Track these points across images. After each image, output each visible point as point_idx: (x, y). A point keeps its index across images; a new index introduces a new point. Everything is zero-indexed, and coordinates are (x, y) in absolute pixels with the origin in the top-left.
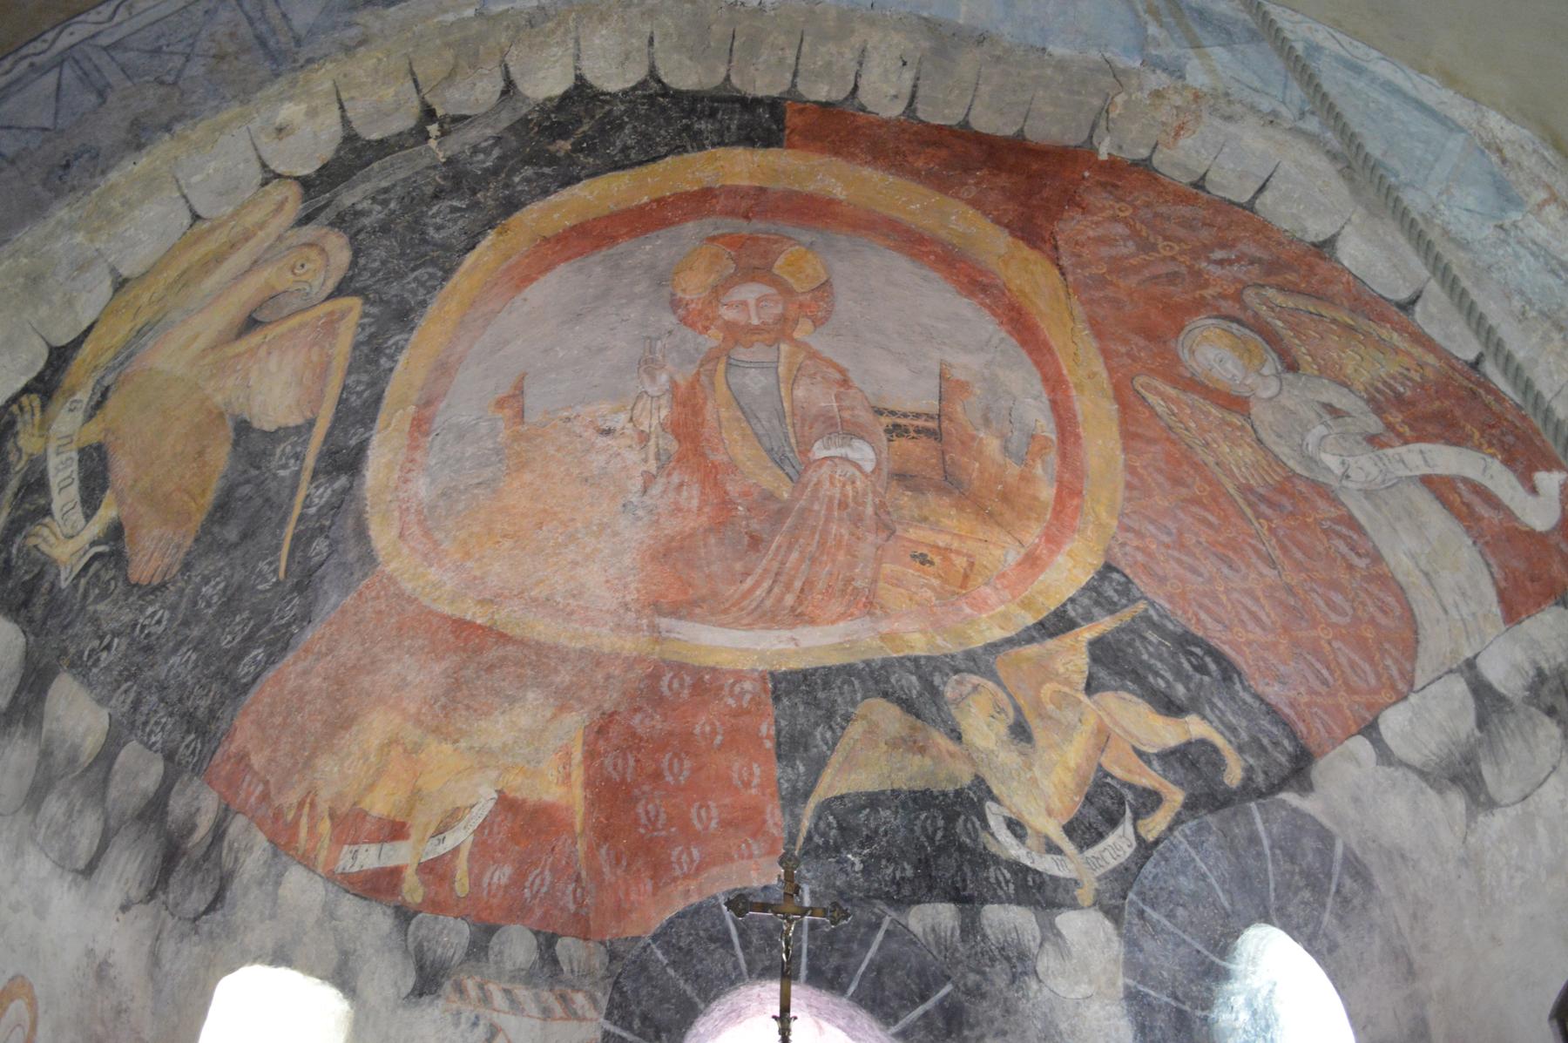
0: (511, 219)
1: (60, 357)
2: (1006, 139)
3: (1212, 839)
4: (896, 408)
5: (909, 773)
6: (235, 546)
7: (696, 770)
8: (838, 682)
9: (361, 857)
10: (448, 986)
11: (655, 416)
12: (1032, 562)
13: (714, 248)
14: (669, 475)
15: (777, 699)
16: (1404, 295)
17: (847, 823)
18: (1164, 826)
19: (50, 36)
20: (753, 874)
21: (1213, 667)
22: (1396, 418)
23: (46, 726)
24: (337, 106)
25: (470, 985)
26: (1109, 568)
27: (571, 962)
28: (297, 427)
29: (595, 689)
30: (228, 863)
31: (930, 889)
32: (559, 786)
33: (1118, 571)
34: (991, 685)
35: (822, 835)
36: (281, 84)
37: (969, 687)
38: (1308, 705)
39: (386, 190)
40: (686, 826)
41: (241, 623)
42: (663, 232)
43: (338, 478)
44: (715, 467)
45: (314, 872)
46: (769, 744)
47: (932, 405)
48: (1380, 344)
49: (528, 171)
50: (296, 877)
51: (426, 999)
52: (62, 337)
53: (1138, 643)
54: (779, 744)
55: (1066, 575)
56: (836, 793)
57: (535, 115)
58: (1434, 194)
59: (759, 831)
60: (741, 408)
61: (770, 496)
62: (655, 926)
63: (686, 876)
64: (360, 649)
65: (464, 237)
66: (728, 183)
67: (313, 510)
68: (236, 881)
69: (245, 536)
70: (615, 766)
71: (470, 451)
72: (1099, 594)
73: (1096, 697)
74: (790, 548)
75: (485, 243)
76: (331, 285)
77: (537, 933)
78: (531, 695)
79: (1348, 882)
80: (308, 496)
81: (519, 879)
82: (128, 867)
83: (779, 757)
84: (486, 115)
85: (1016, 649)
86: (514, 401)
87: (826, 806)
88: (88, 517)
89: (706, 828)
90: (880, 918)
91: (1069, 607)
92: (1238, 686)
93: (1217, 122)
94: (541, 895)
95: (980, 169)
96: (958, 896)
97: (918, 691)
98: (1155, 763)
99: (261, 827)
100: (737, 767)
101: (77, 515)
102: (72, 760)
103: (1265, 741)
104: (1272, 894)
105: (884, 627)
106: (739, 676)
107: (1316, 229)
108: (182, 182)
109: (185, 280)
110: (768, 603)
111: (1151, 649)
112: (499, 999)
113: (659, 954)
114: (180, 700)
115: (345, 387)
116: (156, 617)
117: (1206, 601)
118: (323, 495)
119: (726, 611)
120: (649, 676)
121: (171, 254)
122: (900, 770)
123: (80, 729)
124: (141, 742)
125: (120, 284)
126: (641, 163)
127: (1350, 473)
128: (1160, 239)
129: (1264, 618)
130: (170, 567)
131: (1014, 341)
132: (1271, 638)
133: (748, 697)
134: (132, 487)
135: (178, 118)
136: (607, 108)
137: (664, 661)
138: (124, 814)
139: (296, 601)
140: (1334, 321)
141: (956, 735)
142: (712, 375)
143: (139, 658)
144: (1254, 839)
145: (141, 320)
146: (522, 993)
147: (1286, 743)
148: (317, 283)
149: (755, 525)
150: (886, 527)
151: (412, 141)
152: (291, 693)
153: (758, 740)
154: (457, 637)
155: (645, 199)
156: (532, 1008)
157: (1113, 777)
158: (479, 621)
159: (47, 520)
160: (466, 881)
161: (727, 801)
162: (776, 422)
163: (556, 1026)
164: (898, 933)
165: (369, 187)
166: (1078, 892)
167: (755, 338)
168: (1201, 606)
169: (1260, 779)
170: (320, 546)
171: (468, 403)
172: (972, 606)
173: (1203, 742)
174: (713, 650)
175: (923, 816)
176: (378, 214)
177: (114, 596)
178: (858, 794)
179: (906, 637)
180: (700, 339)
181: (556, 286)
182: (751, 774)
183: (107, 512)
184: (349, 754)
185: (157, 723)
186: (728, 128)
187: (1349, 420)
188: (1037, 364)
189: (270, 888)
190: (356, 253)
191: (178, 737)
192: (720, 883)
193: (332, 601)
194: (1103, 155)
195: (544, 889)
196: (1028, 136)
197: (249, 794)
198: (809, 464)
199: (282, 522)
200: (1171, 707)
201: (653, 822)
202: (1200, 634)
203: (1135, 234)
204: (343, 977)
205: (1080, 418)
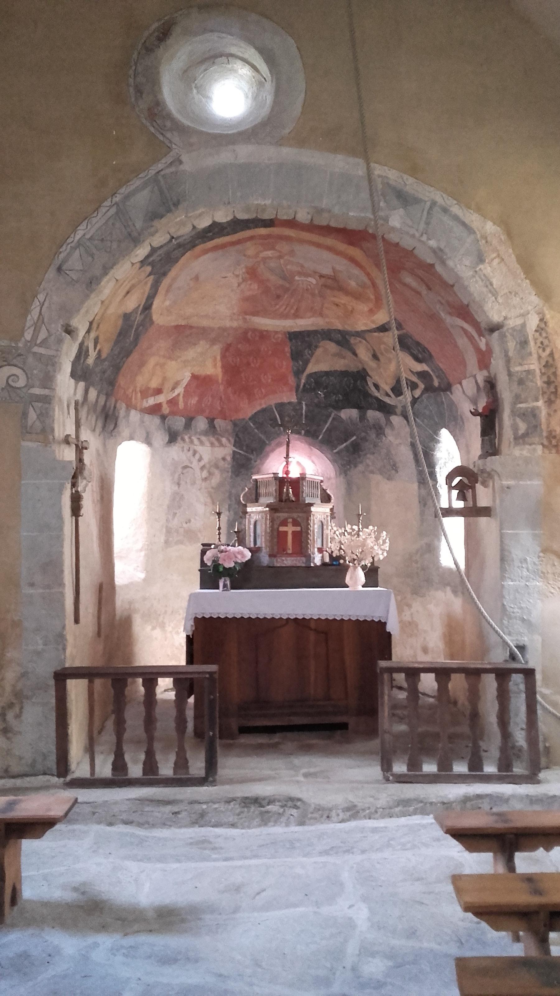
1: (91, 323)
5: (340, 365)
10: (179, 438)
17: (318, 381)
19: (72, 236)
20: (285, 398)
25: (186, 437)
27: (220, 427)
30: (117, 414)
32: (212, 368)
34: (364, 341)
35: (309, 385)
36: (137, 248)
37: (357, 341)
46: (288, 355)
50: (133, 412)
51: (172, 443)
52: (91, 319)
54: (292, 354)
56: (314, 371)
62: (250, 415)
70: (233, 361)
77: (207, 418)
78: (201, 342)
81: (200, 402)
87: (310, 376)
97: (343, 339)
105: (327, 320)
106: (276, 332)
113: (252, 425)
118: (142, 317)
133: (280, 339)
141: (355, 354)
144: (442, 403)
146: (203, 438)
150: (322, 296)
160: (183, 404)
163: (216, 449)
164: (337, 419)
173: (427, 371)
175: (346, 379)
192: (272, 401)
200: (418, 360)
204: (148, 441)
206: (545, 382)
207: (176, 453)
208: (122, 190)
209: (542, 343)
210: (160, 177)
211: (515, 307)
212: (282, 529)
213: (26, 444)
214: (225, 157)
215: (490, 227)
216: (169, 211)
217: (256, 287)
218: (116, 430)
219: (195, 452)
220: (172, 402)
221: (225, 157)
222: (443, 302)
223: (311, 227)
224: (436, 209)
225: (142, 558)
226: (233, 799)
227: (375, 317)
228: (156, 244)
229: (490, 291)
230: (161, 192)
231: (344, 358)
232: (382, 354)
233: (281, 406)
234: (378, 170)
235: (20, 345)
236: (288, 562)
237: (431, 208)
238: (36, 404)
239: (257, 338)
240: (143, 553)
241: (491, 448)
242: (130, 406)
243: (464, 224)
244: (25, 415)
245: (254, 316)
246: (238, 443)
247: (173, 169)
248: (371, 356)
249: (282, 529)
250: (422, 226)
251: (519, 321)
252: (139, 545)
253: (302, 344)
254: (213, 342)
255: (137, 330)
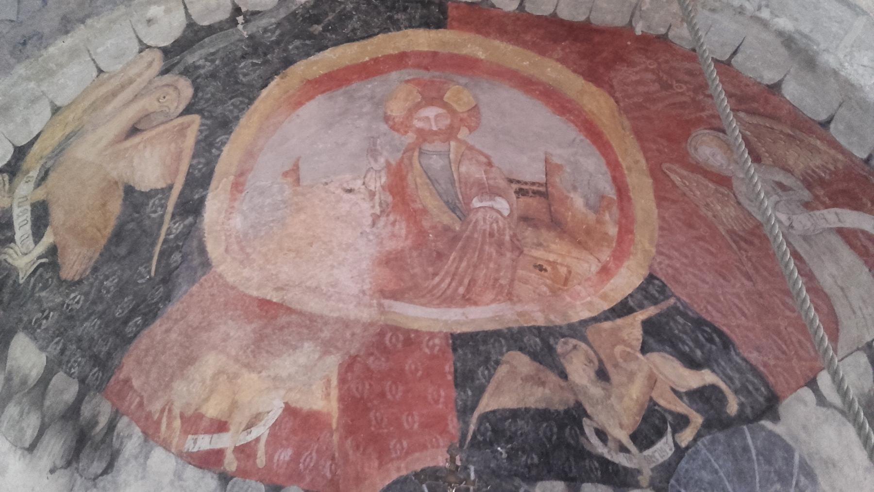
0: (288, 70)
1: (20, 152)
2: (579, 23)
3: (720, 448)
4: (520, 179)
5: (535, 397)
6: (124, 258)
8: (492, 341)
9: (198, 443)
11: (378, 181)
12: (605, 272)
13: (410, 86)
14: (388, 215)
15: (455, 350)
16: (823, 117)
17: (498, 426)
18: (691, 439)
21: (717, 340)
22: (821, 192)
23: (8, 364)
24: (182, 7)
26: (651, 278)
28: (162, 189)
29: (345, 342)
30: (116, 444)
31: (549, 472)
32: (323, 400)
33: (658, 279)
34: (583, 345)
35: (483, 435)
37: (570, 346)
38: (775, 366)
39: (213, 54)
41: (128, 301)
42: (377, 78)
43: (187, 218)
44: (415, 211)
45: (170, 451)
46: (450, 378)
47: (541, 178)
48: (813, 150)
49: (297, 43)
50: (158, 455)
52: (22, 141)
53: (672, 324)
54: (455, 378)
55: (627, 280)
57: (300, 11)
58: (841, 56)
59: (444, 431)
60: (429, 178)
61: (447, 229)
63: (398, 458)
64: (201, 316)
65: (260, 80)
66: (416, 49)
67: (172, 236)
68: (121, 456)
69: (130, 253)
70: (357, 389)
71: (268, 201)
72: (647, 292)
73: (648, 355)
74: (461, 260)
75: (273, 84)
76: (182, 107)
79: (802, 479)
80: (169, 228)
81: (296, 458)
82: (55, 446)
83: (456, 385)
84: (271, 11)
85: (599, 324)
86: (294, 173)
87: (484, 417)
88: (36, 243)
89: (412, 428)
91: (629, 299)
92: (733, 353)
93: (707, 13)
94: (310, 467)
95: (564, 41)
97: (542, 346)
98: (685, 398)
99: (137, 422)
101: (30, 241)
102: (24, 382)
103: (751, 388)
104: (758, 485)
106: (432, 335)
107: (769, 77)
108: (91, 52)
109: (94, 107)
110: (449, 292)
111: (680, 327)
114: (89, 348)
115: (191, 166)
116: (76, 299)
117: (712, 300)
119: (423, 296)
120: (379, 334)
121: (86, 92)
122: (530, 395)
123: (29, 365)
124: (65, 372)
125: (56, 110)
126: (363, 38)
127: (794, 224)
128: (674, 82)
129: (746, 311)
130: (85, 270)
131: (588, 141)
132: (750, 324)
133: (437, 348)
134: (64, 224)
135: (89, 16)
136: (343, 6)
137: (387, 325)
138: (54, 415)
139: (161, 289)
140: (781, 132)
141: (564, 375)
142: (410, 159)
143: (65, 323)
144: (746, 449)
145: (68, 130)
147: (763, 389)
148: (173, 108)
149: (440, 245)
151: (227, 26)
152: (159, 343)
153: (444, 375)
154: (261, 310)
155: (367, 59)
157: (659, 406)
158: (274, 300)
159: (12, 245)
161: (425, 412)
162: (449, 186)
165: (203, 52)
166: (640, 478)
167: (435, 137)
168: (708, 302)
169: (748, 411)
170: (177, 257)
171: (267, 173)
172: (571, 297)
173: (714, 387)
174: (416, 319)
175: (545, 425)
176: (209, 67)
177: (51, 287)
178: (504, 410)
179: (532, 315)
180: (403, 138)
181: (315, 108)
182: (439, 396)
183: (48, 239)
184: (193, 380)
185: (75, 362)
186: (414, 18)
187: (791, 192)
188: (603, 154)
189: (142, 461)
190: (197, 89)
191: (88, 370)
194: (638, 31)
195: (312, 465)
196: (593, 21)
197: (131, 404)
198: (470, 210)
199: (153, 244)
200: (693, 364)
202: (709, 319)
203: (659, 80)
205: (630, 187)
217: (403, 232)
218: (109, 477)
220: (245, 451)
222: (788, 181)
227: (608, 287)
231: (543, 384)
232: (616, 366)
239: (400, 346)
245: (396, 300)
248: (593, 375)
253: (475, 353)
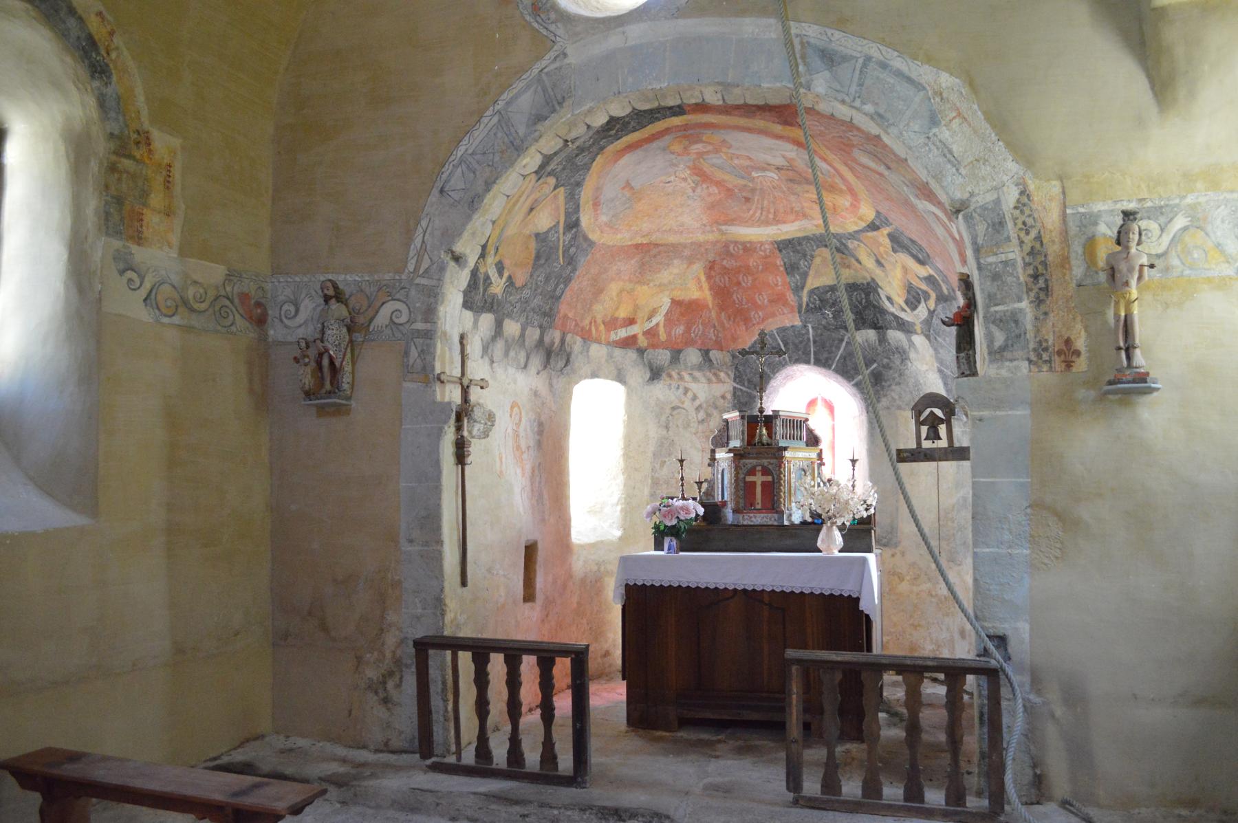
1: (484, 247)
7: (754, 280)
10: (664, 375)
25: (674, 374)
30: (568, 349)
32: (696, 288)
40: (754, 303)
41: (552, 282)
52: (483, 242)
59: (785, 303)
81: (688, 330)
82: (536, 361)
87: (812, 292)
90: (843, 336)
96: (875, 326)
100: (771, 279)
106: (762, 244)
109: (510, 212)
112: (687, 377)
116: (526, 293)
118: (569, 236)
125: (494, 223)
146: (697, 374)
156: (703, 380)
163: (714, 386)
170: (573, 250)
171: (611, 190)
176: (560, 167)
181: (626, 159)
183: (506, 275)
193: (582, 261)
200: (922, 262)
201: (741, 302)
204: (620, 378)
206: (1031, 276)
207: (661, 391)
208: (504, 96)
209: (1024, 223)
210: (544, 77)
211: (984, 179)
212: (749, 479)
213: (408, 385)
214: (614, 41)
215: (946, 80)
216: (554, 111)
219: (686, 390)
221: (614, 41)
223: (727, 109)
224: (872, 65)
225: (618, 513)
226: (590, 808)
228: (548, 150)
229: (949, 161)
230: (545, 91)
233: (782, 330)
234: (795, 29)
235: (403, 277)
236: (758, 519)
237: (865, 65)
238: (418, 341)
240: (619, 508)
241: (967, 367)
242: (587, 337)
243: (909, 80)
244: (406, 354)
246: (738, 378)
247: (557, 64)
249: (749, 479)
250: (854, 88)
251: (990, 197)
252: (615, 499)
253: (795, 253)
254: (690, 261)
255: (566, 251)
